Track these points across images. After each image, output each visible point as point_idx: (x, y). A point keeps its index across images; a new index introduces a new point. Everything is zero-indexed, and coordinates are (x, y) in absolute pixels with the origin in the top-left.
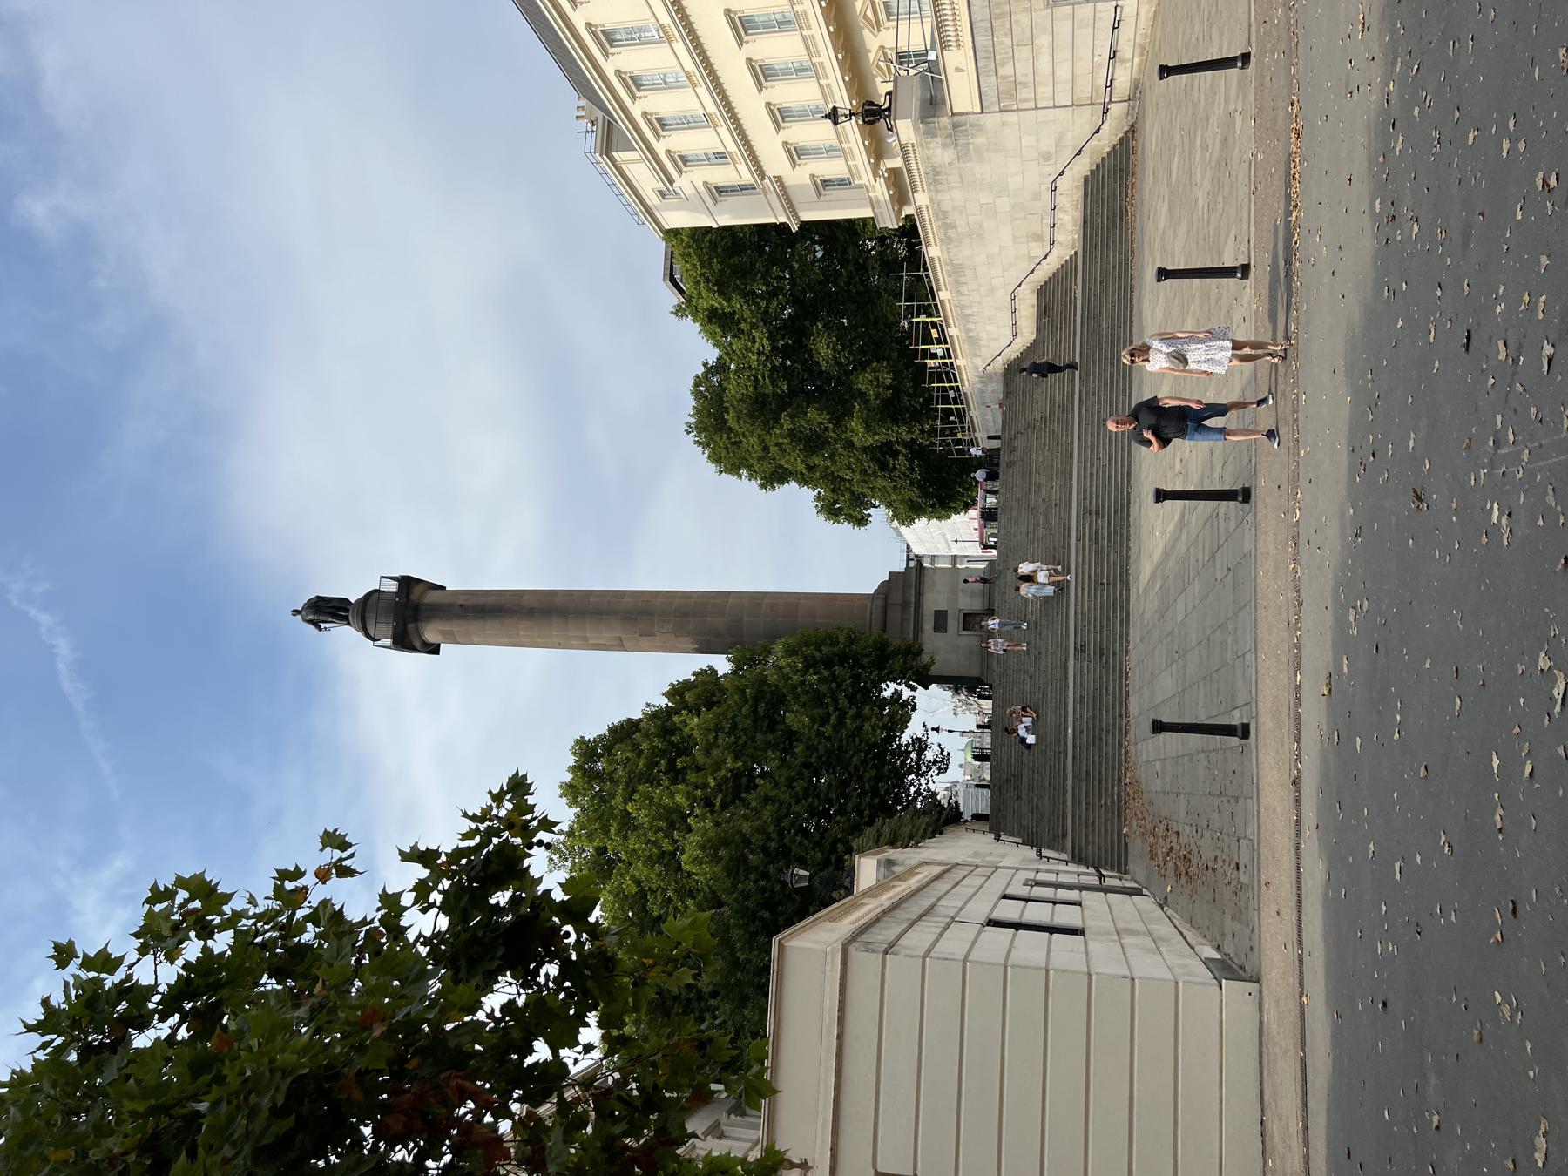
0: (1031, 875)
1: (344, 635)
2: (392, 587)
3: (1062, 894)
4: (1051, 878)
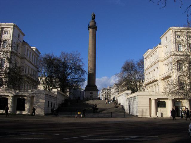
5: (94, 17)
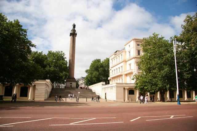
1: (72, 28)
5: (74, 26)
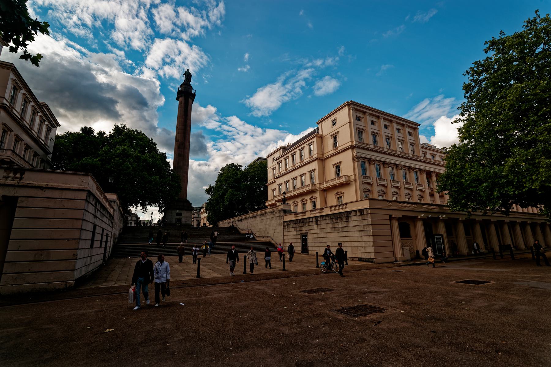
0: (110, 235)
2: (193, 92)
3: (104, 243)
4: (109, 240)
